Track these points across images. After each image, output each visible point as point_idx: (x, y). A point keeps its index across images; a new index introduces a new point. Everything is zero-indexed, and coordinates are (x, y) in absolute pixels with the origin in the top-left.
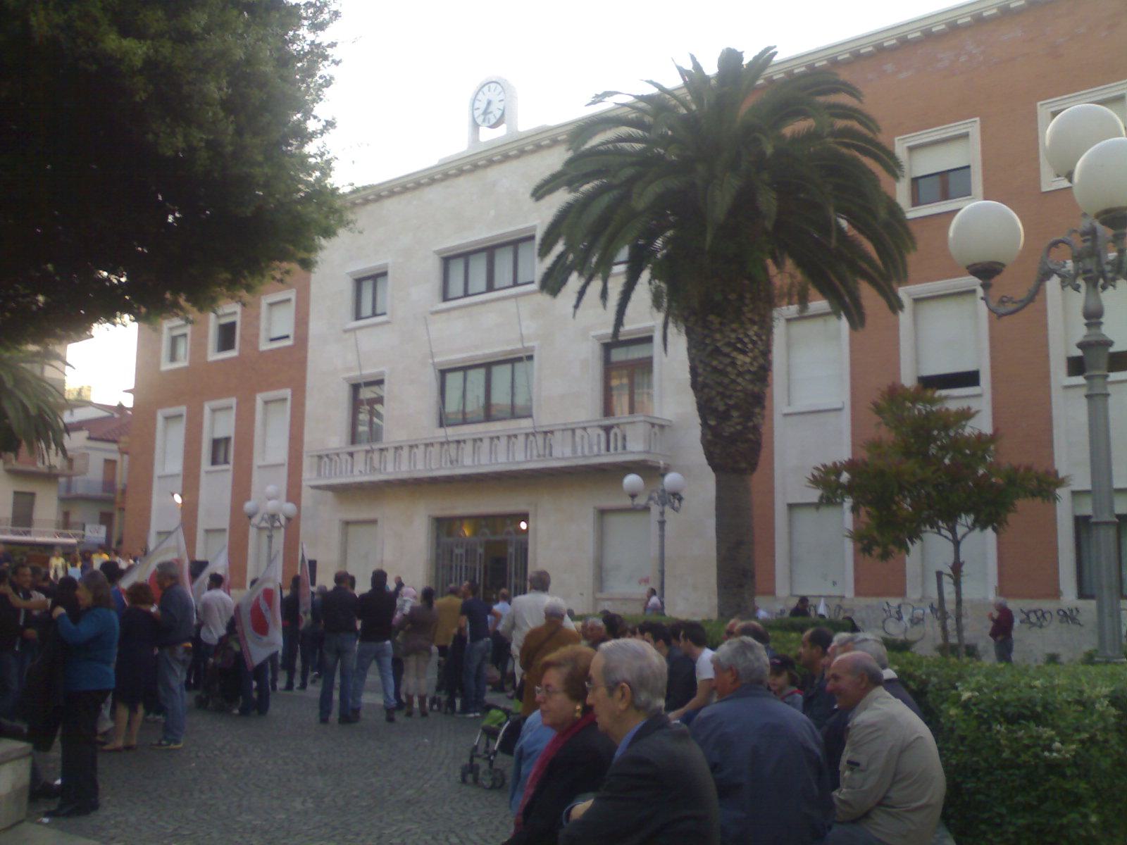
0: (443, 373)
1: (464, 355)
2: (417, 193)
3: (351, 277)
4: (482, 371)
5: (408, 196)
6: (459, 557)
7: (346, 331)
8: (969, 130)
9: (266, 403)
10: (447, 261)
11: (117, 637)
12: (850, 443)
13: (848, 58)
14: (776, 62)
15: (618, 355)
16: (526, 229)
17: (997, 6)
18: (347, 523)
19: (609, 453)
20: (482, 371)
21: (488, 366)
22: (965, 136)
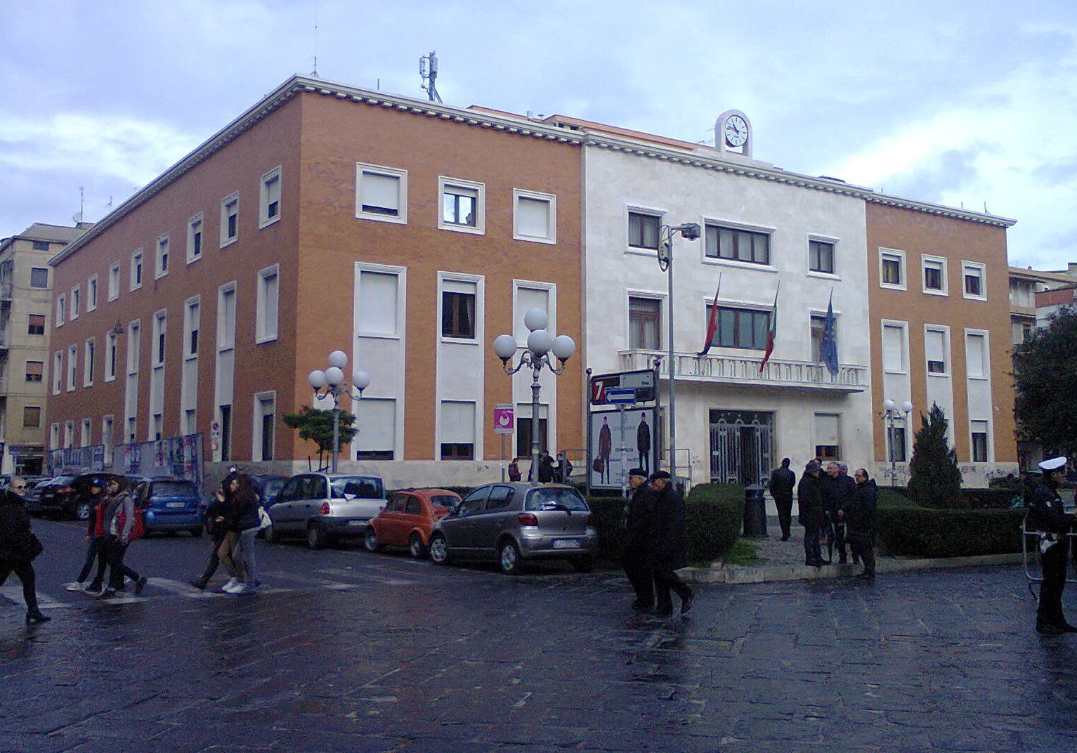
12: (354, 360)
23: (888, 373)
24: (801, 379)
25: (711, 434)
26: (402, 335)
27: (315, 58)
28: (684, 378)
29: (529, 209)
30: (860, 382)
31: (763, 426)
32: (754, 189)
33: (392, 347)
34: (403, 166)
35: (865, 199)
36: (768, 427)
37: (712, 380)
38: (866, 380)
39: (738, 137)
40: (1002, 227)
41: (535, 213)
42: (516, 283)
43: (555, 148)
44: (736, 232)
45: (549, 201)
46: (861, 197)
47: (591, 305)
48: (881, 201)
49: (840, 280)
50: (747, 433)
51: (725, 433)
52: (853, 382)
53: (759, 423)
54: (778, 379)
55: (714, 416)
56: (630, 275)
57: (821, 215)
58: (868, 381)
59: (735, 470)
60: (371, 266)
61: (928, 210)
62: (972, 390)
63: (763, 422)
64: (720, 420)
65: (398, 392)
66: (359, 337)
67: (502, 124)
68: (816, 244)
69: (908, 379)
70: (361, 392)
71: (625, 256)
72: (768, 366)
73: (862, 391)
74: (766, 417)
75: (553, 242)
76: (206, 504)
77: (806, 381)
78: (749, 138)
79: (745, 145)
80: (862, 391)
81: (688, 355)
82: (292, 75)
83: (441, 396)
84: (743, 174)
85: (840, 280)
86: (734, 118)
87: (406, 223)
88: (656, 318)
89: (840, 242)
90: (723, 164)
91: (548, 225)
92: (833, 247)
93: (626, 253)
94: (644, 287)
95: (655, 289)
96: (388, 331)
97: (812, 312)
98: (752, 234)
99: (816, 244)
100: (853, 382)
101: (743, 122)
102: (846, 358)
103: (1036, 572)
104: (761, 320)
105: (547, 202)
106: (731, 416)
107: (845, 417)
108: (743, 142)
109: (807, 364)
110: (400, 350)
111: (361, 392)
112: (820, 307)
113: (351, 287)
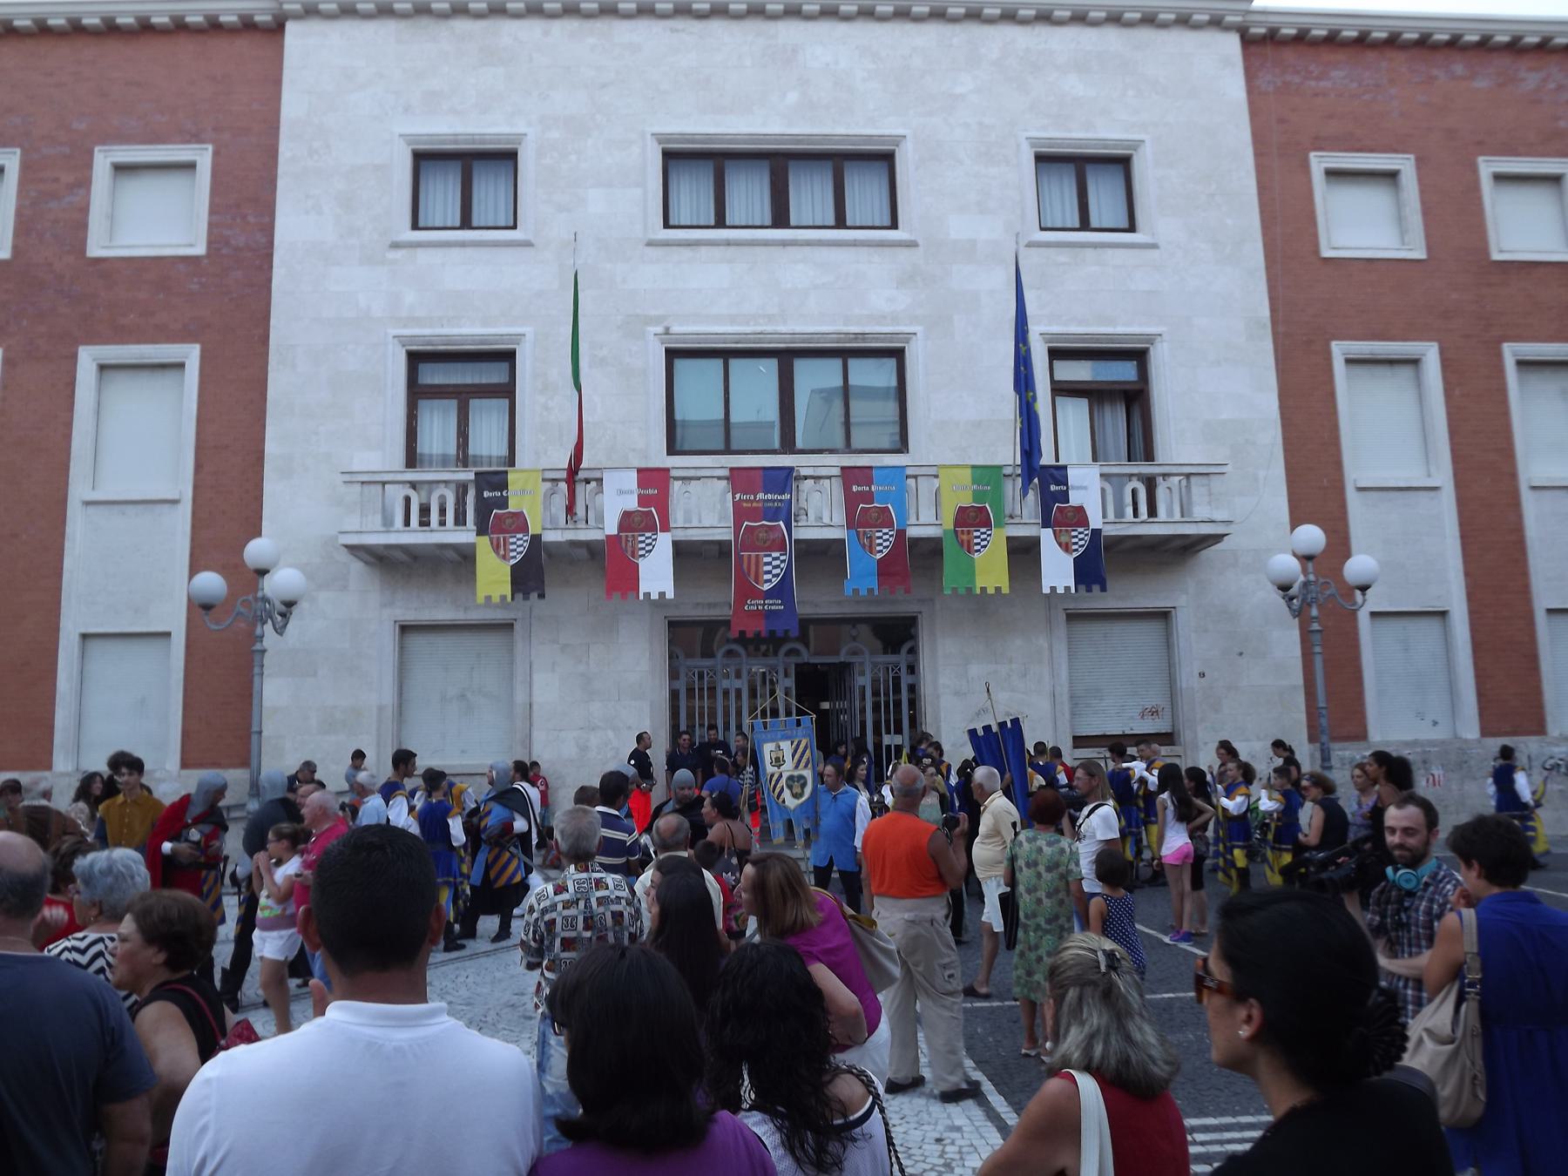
0: (898, 354)
1: (427, 331)
2: (600, 25)
3: (1033, 146)
4: (769, 367)
5: (1146, 34)
6: (733, 695)
7: (650, 244)
8: (197, 158)
9: (103, 368)
10: (425, 159)
11: (965, 905)
12: (1457, 534)
13: (62, 26)
14: (1255, 10)
15: (433, 375)
16: (881, 138)
17: (1359, 28)
18: (405, 629)
19: (407, 529)
20: (769, 367)
21: (786, 357)
22: (190, 166)
29: (140, 190)
30: (1200, 512)
36: (902, 658)
41: (1372, 199)
43: (219, 47)
49: (1154, 246)
54: (1177, 517)
56: (410, 297)
57: (1074, 85)
69: (186, 510)
75: (1420, 254)
76: (808, 827)
77: (584, 526)
85: (1154, 246)
88: (1135, 399)
89: (1148, 144)
91: (1400, 219)
93: (396, 246)
103: (941, 1161)
107: (1184, 621)
110: (1446, 507)
113: (1502, 391)
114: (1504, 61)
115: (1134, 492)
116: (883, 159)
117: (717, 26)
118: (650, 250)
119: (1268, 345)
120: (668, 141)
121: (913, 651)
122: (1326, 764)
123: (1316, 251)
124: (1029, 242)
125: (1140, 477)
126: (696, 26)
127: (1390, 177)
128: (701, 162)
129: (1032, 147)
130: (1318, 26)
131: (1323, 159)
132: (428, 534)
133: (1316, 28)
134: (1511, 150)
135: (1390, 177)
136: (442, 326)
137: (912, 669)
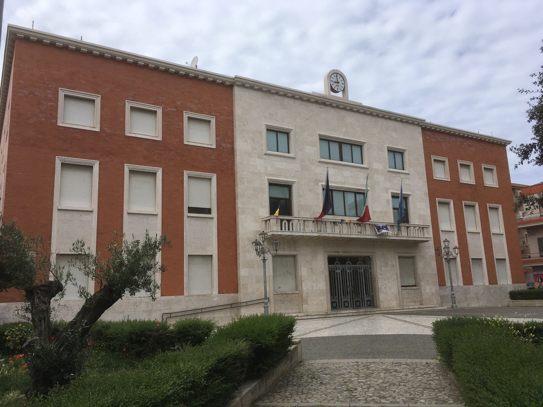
1: (278, 178)
23: (443, 231)
24: (401, 235)
25: (330, 272)
26: (95, 207)
27: (33, 22)
28: (307, 234)
31: (343, 266)
32: (351, 118)
33: (85, 217)
34: (97, 92)
35: (421, 126)
37: (327, 235)
38: (429, 234)
39: (339, 86)
40: (503, 145)
42: (186, 173)
44: (341, 143)
45: (445, 161)
46: (418, 125)
47: (240, 188)
48: (489, 140)
50: (355, 273)
51: (340, 271)
52: (421, 236)
53: (362, 264)
55: (331, 260)
56: (269, 169)
58: (431, 235)
59: (348, 295)
60: (127, 164)
61: (489, 140)
62: (495, 241)
63: (364, 263)
64: (359, 262)
65: (213, 250)
66: (59, 210)
67: (336, 104)
68: (392, 151)
69: (95, 216)
70: (276, 252)
71: (264, 156)
72: (365, 226)
73: (428, 241)
74: (367, 260)
78: (345, 87)
79: (344, 91)
80: (428, 241)
81: (309, 219)
82: (511, 140)
83: (188, 251)
84: (400, 120)
85: (409, 174)
86: (335, 74)
87: (99, 131)
90: (350, 105)
92: (289, 134)
94: (279, 176)
95: (286, 177)
96: (84, 205)
97: (392, 193)
98: (352, 144)
99: (392, 151)
100: (421, 236)
101: (341, 77)
102: (414, 219)
104: (362, 196)
105: (209, 121)
106: (343, 260)
108: (342, 89)
109: (390, 224)
110: (93, 220)
111: (276, 252)
112: (397, 190)
114: (461, 140)
115: (285, 223)
116: (360, 146)
117: (389, 121)
118: (319, 164)
119: (428, 198)
120: (321, 136)
121: (370, 264)
122: (452, 290)
123: (433, 177)
124: (319, 161)
125: (287, 220)
126: (280, 98)
127: (443, 162)
128: (274, 132)
129: (266, 127)
130: (19, 33)
131: (188, 114)
132: (282, 232)
133: (140, 62)
134: (61, 88)
135: (443, 162)
136: (277, 177)
137: (370, 268)
